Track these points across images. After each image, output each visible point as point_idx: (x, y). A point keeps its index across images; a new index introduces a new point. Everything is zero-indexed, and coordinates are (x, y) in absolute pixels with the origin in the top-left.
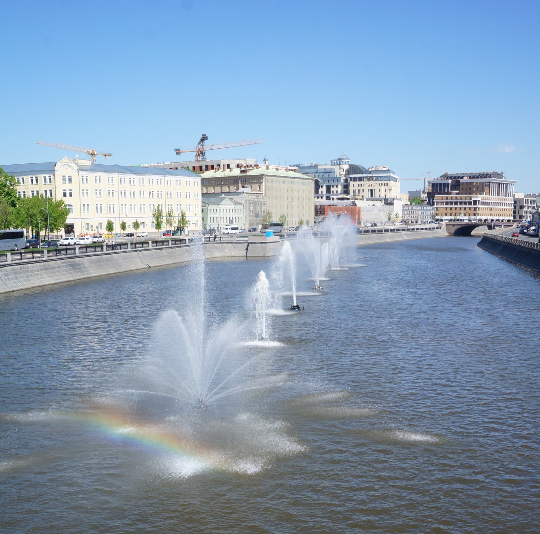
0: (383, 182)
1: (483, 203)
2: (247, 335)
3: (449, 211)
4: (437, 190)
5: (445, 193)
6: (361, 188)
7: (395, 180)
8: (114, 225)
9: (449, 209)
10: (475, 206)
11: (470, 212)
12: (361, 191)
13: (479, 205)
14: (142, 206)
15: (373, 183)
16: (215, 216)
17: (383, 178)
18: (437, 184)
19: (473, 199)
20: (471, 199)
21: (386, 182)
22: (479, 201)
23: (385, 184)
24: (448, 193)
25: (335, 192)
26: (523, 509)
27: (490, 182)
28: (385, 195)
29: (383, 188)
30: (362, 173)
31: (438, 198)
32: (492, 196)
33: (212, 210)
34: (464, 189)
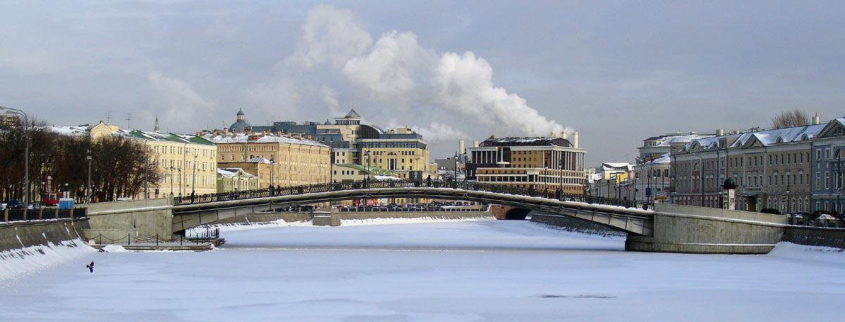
0: (408, 150)
4: (479, 161)
6: (379, 157)
11: (520, 163)
12: (378, 161)
13: (536, 181)
14: (205, 164)
16: (534, 182)
18: (479, 152)
19: (528, 173)
20: (525, 172)
21: (411, 150)
22: (536, 176)
23: (348, 172)
25: (341, 162)
27: (551, 151)
28: (411, 167)
29: (407, 158)
32: (555, 170)
34: (517, 159)
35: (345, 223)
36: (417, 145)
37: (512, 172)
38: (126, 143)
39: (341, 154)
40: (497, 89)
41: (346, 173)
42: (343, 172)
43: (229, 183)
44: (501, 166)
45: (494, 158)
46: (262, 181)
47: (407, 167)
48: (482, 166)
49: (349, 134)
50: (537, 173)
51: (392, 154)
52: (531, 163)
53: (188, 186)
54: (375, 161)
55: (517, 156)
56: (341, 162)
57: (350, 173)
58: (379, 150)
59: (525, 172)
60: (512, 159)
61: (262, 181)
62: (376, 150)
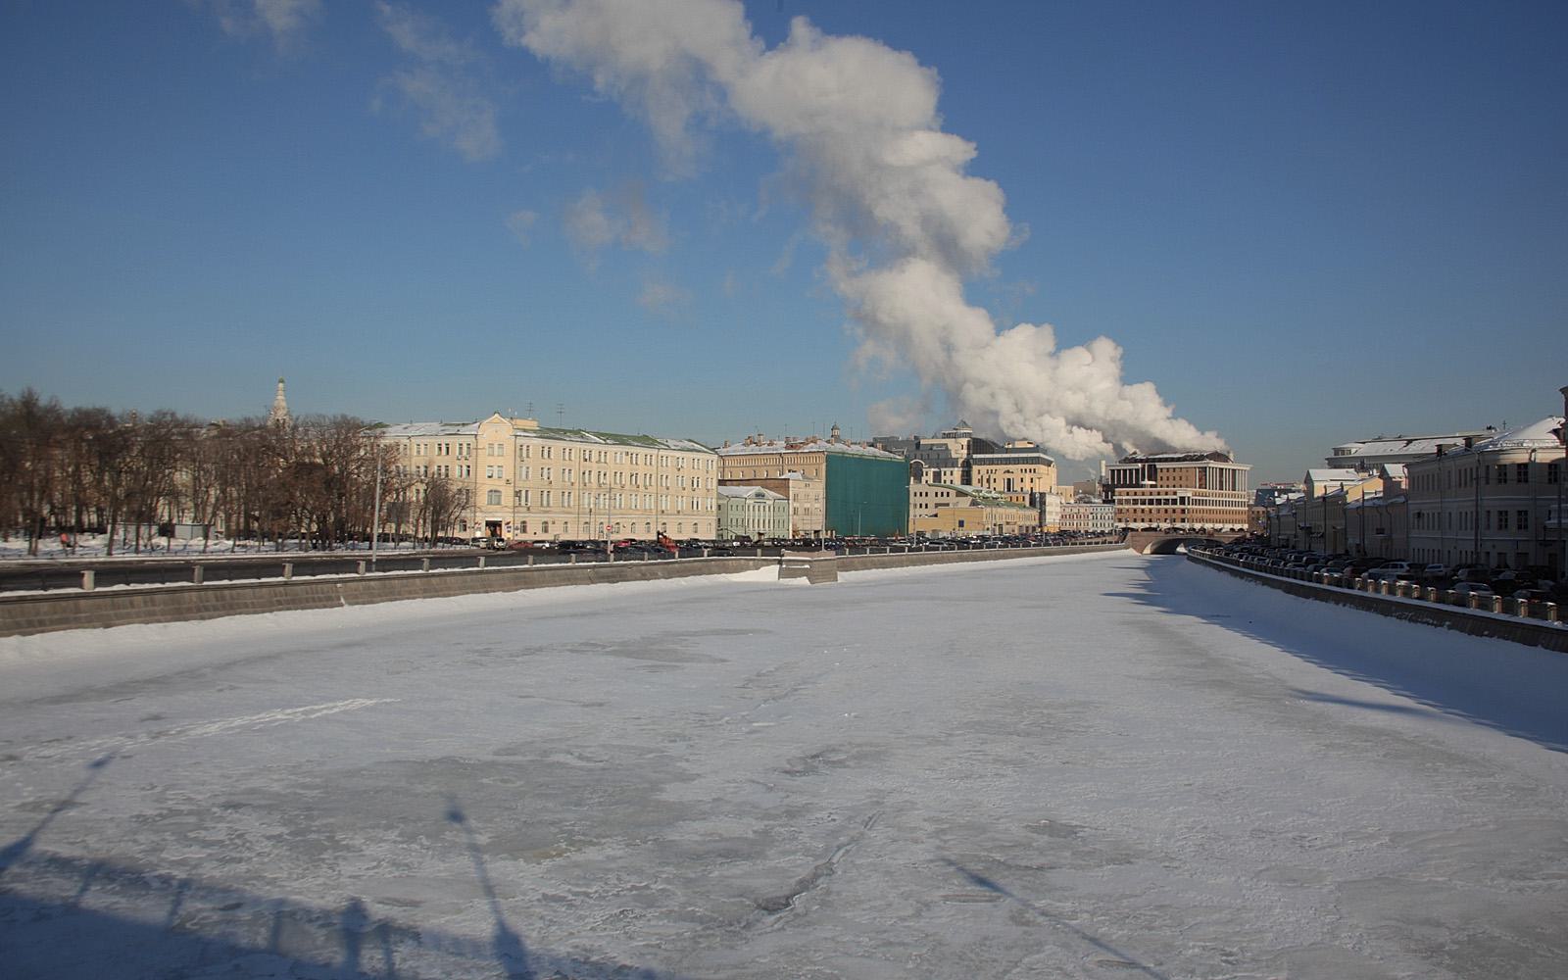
1: (1196, 502)
2: (246, 465)
3: (1163, 515)
5: (1131, 486)
7: (1049, 464)
8: (43, 401)
9: (1139, 513)
10: (1183, 507)
11: (1143, 516)
12: (992, 481)
15: (1011, 467)
16: (1186, 506)
17: (1026, 461)
19: (1179, 495)
20: (1175, 493)
21: (1032, 467)
24: (1138, 485)
25: (948, 483)
26: (591, 841)
29: (1027, 477)
30: (993, 453)
31: (1120, 493)
33: (734, 508)
34: (1165, 478)
35: (843, 577)
36: (1037, 461)
37: (1159, 494)
38: (388, 449)
39: (948, 473)
40: (1126, 387)
41: (939, 495)
42: (936, 494)
43: (740, 508)
44: (1142, 486)
45: (1137, 478)
46: (796, 505)
47: (1027, 488)
48: (1124, 486)
49: (959, 449)
50: (1190, 495)
51: (1008, 472)
52: (1181, 482)
53: (663, 512)
54: (988, 481)
55: (1164, 475)
56: (948, 483)
57: (945, 494)
58: (993, 467)
59: (1175, 493)
60: (1159, 478)
61: (796, 505)
62: (990, 467)
